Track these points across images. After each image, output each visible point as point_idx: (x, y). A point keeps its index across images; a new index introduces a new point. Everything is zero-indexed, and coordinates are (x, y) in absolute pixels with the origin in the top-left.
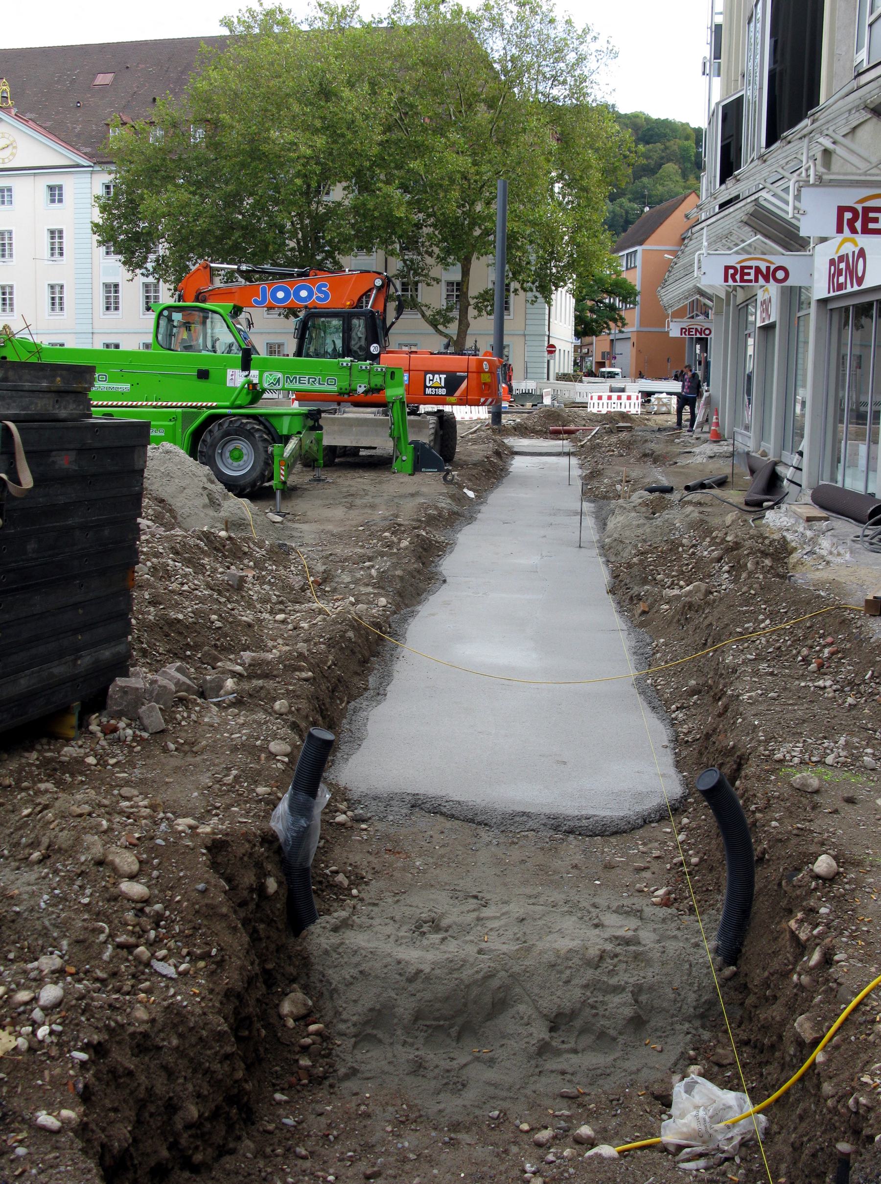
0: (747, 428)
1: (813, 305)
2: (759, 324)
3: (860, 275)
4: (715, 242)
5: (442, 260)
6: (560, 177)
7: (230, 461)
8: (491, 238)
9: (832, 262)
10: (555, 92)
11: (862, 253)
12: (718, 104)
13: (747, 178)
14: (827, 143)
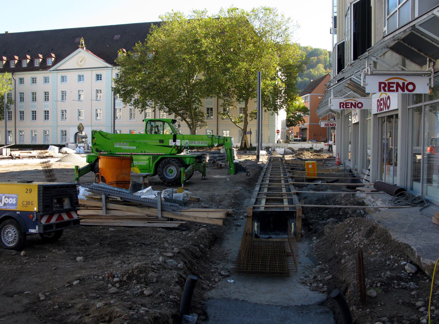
0: (350, 160)
1: (372, 116)
2: (353, 122)
3: (388, 105)
4: (336, 93)
5: (238, 100)
6: (280, 70)
7: (170, 174)
8: (256, 92)
9: (378, 101)
10: (278, 40)
11: (389, 98)
12: (336, 44)
13: (347, 72)
14: (374, 59)
